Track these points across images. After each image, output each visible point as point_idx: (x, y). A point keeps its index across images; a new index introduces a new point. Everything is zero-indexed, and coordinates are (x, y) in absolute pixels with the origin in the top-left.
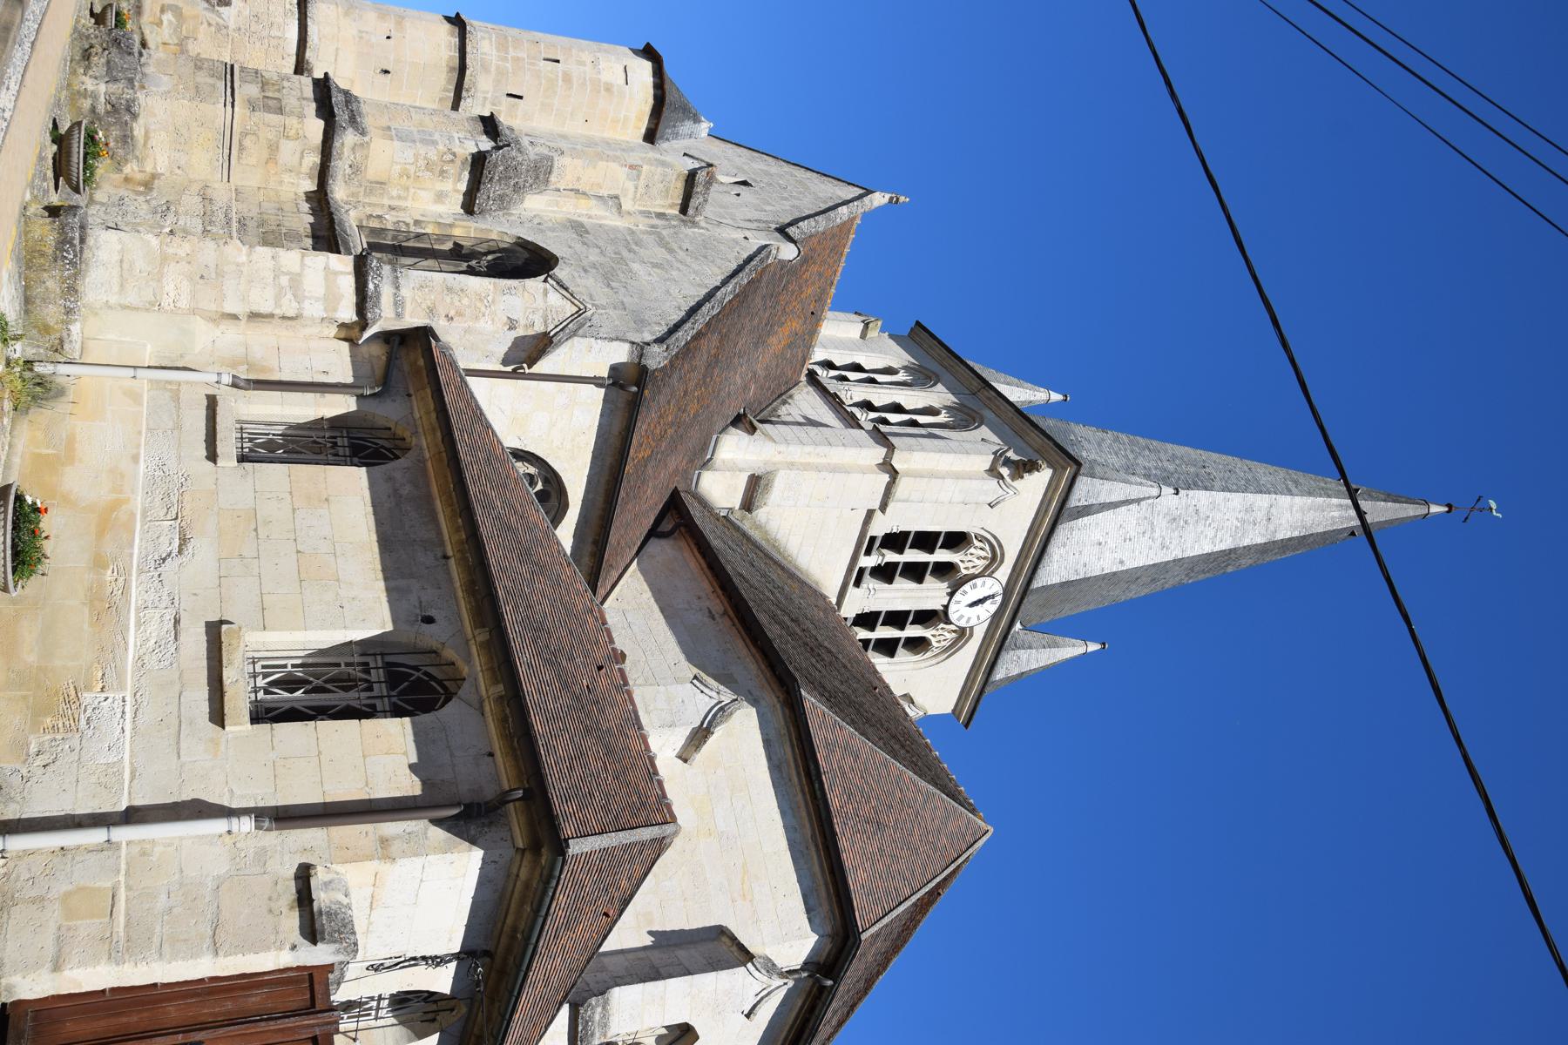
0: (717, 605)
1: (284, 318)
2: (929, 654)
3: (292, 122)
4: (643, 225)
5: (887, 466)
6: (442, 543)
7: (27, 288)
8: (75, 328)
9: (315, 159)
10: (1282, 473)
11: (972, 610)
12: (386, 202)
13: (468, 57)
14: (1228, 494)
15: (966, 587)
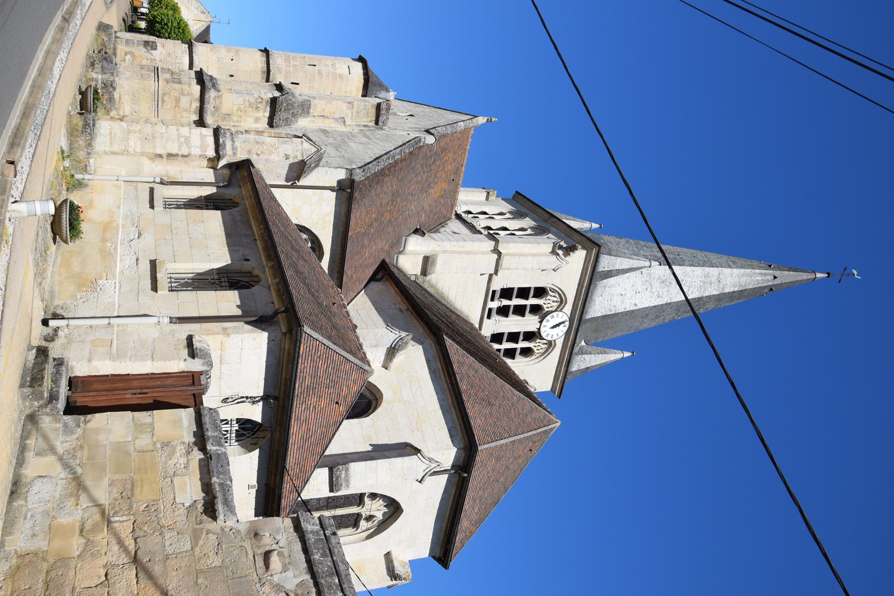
0: (404, 306)
1: (183, 156)
2: (533, 357)
3: (186, 87)
4: (356, 130)
5: (496, 251)
6: (254, 235)
7: (71, 144)
8: (92, 161)
9: (197, 104)
10: (725, 258)
11: (554, 329)
12: (232, 124)
14: (693, 268)
15: (548, 317)
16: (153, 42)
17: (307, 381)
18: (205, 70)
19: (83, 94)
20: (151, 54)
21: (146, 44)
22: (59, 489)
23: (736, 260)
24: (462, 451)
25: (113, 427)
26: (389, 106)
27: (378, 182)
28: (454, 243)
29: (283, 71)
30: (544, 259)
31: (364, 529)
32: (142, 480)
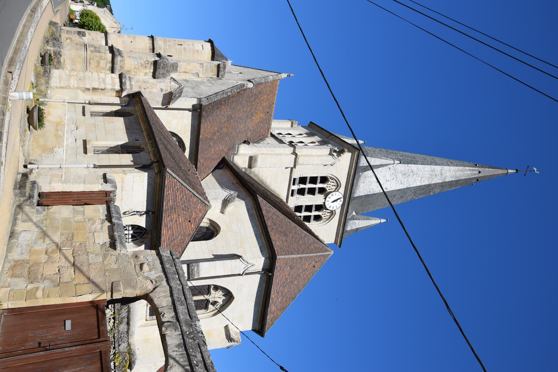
0: (235, 182)
1: (102, 89)
2: (322, 221)
3: (103, 55)
4: (205, 80)
5: (294, 153)
8: (49, 91)
9: (110, 65)
10: (446, 160)
15: (330, 195)
16: (83, 32)
17: (171, 203)
18: (115, 46)
19: (43, 57)
21: (79, 33)
22: (35, 236)
23: (454, 161)
24: (268, 260)
25: (63, 212)
26: (225, 66)
27: (218, 108)
28: (268, 149)
30: (325, 158)
31: (211, 310)
32: (78, 233)
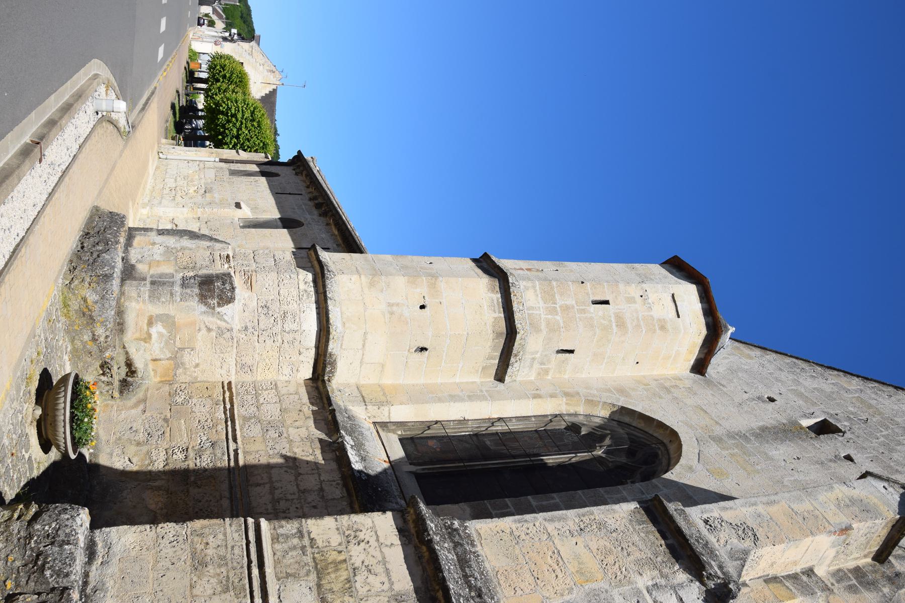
13: (517, 316)
20: (220, 317)
29: (543, 326)
